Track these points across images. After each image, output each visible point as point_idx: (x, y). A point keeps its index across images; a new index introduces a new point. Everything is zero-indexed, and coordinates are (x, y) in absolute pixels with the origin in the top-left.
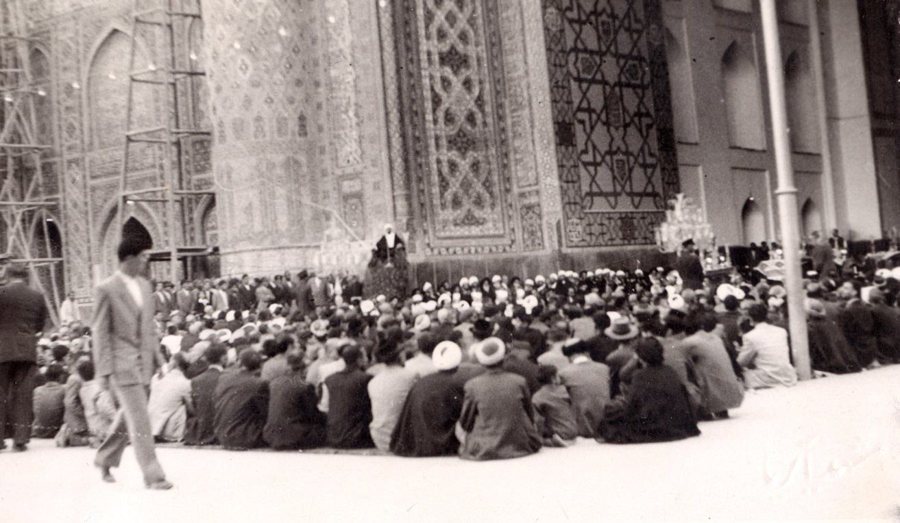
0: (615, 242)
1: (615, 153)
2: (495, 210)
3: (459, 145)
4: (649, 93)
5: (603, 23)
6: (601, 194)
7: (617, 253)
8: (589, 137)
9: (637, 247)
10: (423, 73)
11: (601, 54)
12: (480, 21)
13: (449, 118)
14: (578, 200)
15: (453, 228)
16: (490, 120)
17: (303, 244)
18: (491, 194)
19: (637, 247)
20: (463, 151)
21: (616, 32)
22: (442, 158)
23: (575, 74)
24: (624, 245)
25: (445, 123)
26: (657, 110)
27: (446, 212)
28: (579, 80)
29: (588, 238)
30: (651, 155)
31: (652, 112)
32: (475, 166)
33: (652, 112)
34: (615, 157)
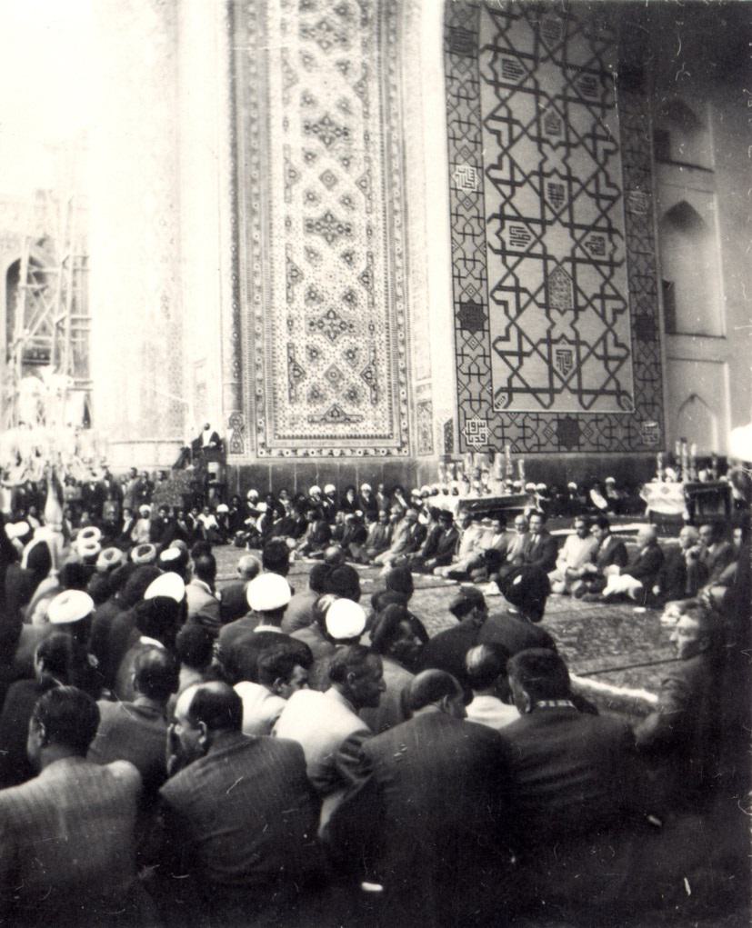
2: (380, 405)
3: (327, 328)
4: (622, 272)
5: (551, 186)
6: (528, 390)
7: (546, 462)
8: (506, 151)
9: (582, 456)
10: (276, 242)
11: (543, 222)
12: (377, 185)
13: (312, 296)
14: (485, 396)
15: (306, 425)
16: (380, 300)
17: (156, 439)
18: (374, 388)
19: (582, 456)
20: (333, 337)
21: (572, 199)
22: (296, 342)
23: (497, 245)
24: (559, 451)
25: (306, 301)
26: (633, 292)
27: (296, 406)
28: (503, 253)
30: (617, 344)
31: (625, 293)
32: (351, 354)
33: (625, 293)
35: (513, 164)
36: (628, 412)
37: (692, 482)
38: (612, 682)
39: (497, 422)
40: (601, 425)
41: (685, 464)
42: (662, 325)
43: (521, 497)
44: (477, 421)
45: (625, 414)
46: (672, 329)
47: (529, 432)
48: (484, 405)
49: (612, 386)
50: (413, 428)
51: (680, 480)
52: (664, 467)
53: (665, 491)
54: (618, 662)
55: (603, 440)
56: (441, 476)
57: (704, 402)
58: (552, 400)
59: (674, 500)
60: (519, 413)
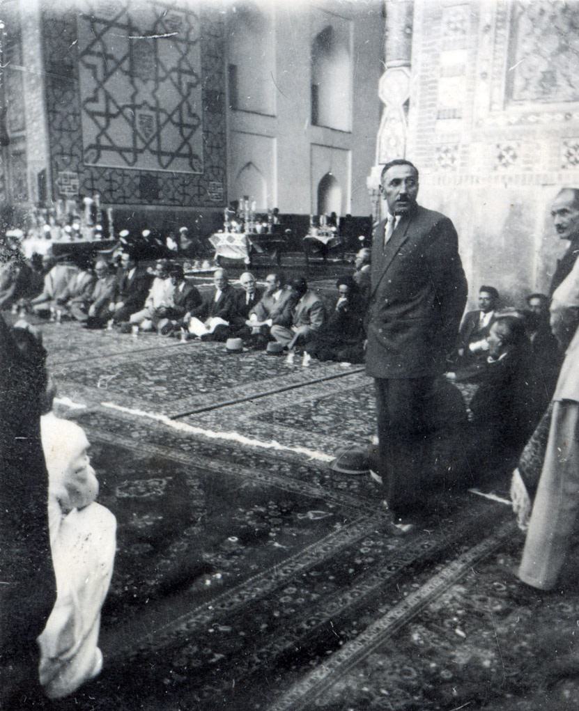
1: (139, 107)
6: (112, 148)
8: (100, 84)
9: (161, 208)
14: (76, 150)
24: (142, 204)
26: (205, 69)
34: (138, 112)
35: (108, 97)
36: (198, 173)
37: (252, 233)
38: (204, 424)
39: (87, 175)
40: (177, 183)
41: (247, 218)
42: (227, 99)
43: (109, 242)
44: (69, 173)
45: (195, 175)
46: (235, 109)
47: (115, 185)
48: (75, 160)
49: (185, 150)
50: (9, 176)
51: (242, 231)
52: (230, 220)
53: (231, 239)
54: (206, 400)
55: (177, 196)
56: (34, 221)
57: (258, 170)
58: (135, 160)
59: (238, 247)
60: (106, 168)
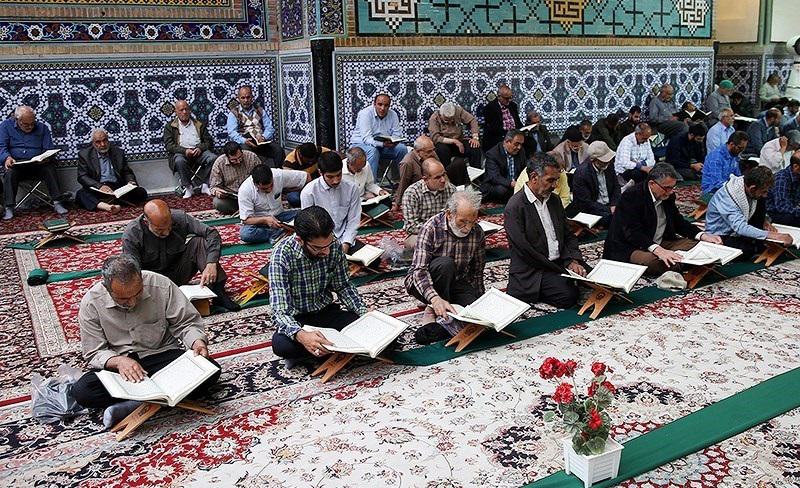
0: (521, 28)
29: (627, 20)
